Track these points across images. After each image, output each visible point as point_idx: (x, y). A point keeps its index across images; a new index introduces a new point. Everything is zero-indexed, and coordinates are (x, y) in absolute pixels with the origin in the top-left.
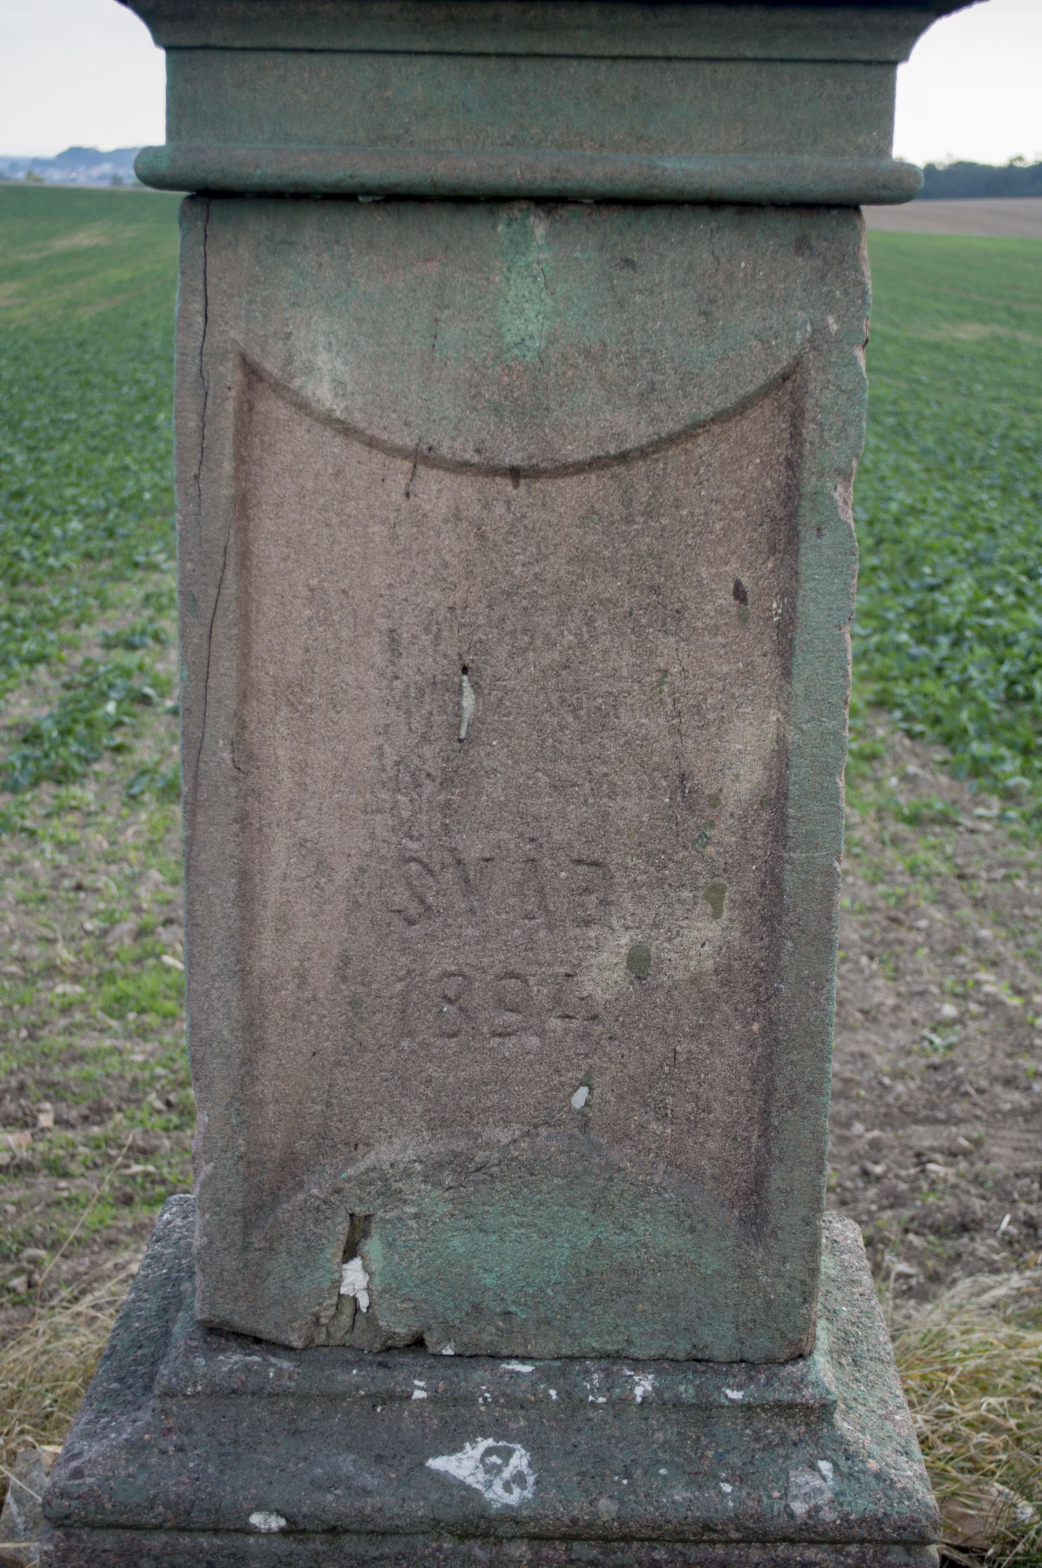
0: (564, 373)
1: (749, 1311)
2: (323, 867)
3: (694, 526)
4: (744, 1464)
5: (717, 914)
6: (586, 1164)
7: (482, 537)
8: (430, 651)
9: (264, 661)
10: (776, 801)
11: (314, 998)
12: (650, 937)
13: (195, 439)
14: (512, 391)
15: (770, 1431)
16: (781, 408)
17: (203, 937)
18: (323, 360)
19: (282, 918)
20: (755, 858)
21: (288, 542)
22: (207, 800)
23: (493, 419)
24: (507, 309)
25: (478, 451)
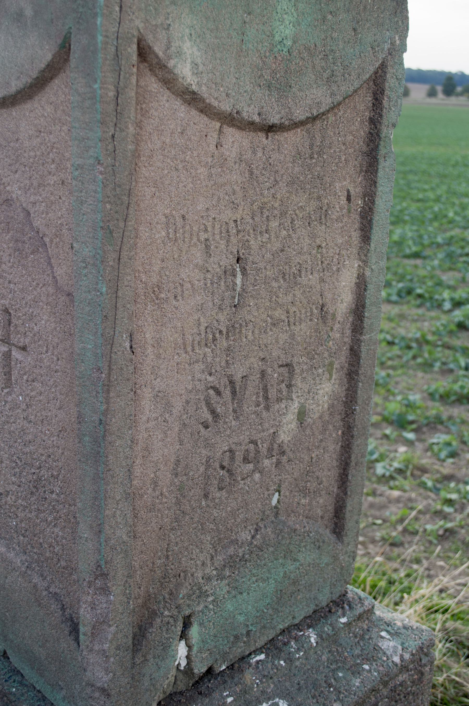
1: (335, 576)
2: (168, 406)
3: (335, 159)
4: (361, 651)
5: (330, 379)
7: (251, 173)
10: (359, 310)
11: (162, 494)
13: (112, 106)
14: (276, 74)
15: (357, 630)
17: (113, 477)
19: (146, 449)
20: (345, 343)
22: (116, 380)
24: (277, 18)
25: (259, 114)
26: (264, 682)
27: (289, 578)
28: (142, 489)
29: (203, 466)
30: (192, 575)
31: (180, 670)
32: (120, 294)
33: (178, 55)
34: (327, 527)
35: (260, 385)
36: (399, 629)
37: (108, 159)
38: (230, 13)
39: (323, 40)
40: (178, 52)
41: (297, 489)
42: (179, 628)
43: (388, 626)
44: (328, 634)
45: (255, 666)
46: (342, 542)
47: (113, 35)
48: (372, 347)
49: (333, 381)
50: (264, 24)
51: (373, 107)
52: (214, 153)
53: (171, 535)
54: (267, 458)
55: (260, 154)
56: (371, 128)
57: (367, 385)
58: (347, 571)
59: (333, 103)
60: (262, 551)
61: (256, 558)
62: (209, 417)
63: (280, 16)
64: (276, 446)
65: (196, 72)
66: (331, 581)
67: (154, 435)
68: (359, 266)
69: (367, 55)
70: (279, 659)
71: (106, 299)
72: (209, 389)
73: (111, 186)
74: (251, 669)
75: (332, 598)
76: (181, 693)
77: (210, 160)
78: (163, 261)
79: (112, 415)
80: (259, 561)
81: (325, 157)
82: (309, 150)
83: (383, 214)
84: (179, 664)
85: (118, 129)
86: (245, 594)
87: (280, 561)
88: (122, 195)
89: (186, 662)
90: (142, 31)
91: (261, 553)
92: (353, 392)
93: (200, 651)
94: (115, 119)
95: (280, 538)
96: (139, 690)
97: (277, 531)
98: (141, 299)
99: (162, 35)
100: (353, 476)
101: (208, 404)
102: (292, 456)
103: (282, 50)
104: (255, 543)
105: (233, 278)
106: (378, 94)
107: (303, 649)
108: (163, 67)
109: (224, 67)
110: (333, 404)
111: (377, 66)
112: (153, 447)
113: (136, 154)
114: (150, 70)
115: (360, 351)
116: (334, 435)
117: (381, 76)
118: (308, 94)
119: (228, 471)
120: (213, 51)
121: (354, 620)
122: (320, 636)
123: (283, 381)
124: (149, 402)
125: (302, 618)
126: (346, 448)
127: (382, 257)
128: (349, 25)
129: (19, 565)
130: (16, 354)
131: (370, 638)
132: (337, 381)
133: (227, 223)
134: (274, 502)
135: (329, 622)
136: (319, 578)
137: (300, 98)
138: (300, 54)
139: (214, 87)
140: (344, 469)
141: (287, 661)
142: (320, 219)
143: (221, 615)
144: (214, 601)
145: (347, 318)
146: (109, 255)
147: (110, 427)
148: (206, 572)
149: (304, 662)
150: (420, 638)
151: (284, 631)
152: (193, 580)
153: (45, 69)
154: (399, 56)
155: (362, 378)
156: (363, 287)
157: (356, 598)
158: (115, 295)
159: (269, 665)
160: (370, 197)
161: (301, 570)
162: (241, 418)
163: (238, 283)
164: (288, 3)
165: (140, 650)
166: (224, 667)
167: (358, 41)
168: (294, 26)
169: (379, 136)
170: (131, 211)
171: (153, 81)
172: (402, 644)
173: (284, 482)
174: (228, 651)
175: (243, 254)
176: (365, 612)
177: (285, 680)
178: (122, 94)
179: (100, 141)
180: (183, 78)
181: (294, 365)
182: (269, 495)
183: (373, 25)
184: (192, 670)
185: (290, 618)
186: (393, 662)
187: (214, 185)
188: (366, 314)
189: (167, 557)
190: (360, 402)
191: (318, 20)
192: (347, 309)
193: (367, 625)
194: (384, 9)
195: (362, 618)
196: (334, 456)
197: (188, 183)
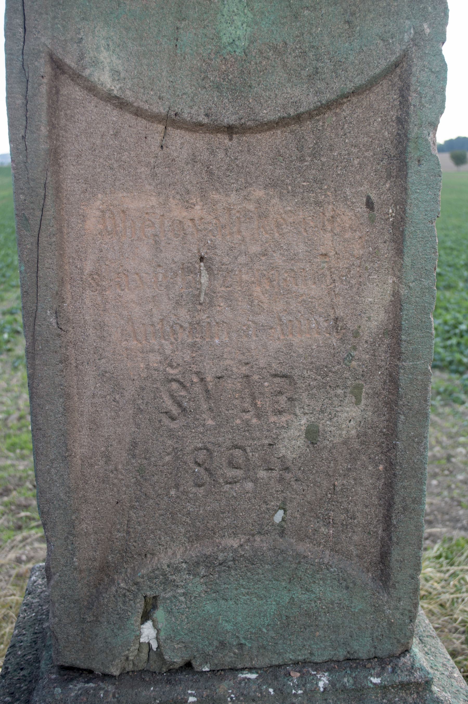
0: (261, 62)
1: (380, 630)
3: (341, 162)
5: (358, 402)
6: (284, 555)
7: (210, 173)
8: (180, 248)
9: (74, 259)
10: (394, 331)
11: (116, 470)
12: (319, 418)
14: (228, 75)
15: (397, 699)
16: (393, 85)
17: (44, 436)
18: (104, 56)
20: (380, 367)
24: (223, 20)
25: (207, 115)
30: (158, 559)
32: (40, 274)
33: (93, 64)
39: (297, 36)
49: (362, 406)
51: (400, 105)
52: (157, 154)
58: (401, 630)
62: (175, 411)
65: (117, 78)
66: (372, 634)
67: (102, 411)
68: (394, 282)
69: (372, 47)
70: (270, 686)
77: (152, 160)
90: (49, 46)
94: (25, 123)
96: (91, 647)
101: (172, 396)
102: (300, 474)
107: (304, 688)
108: (79, 76)
112: (102, 423)
114: (72, 80)
117: (406, 70)
119: (206, 469)
135: (354, 675)
137: (265, 97)
142: (323, 226)
143: (197, 612)
144: (184, 594)
146: (25, 239)
156: (399, 306)
164: (238, 4)
169: (406, 136)
171: (77, 89)
178: (31, 102)
180: (102, 85)
181: (295, 378)
187: (159, 184)
189: (128, 533)
193: (413, 699)
195: (409, 689)
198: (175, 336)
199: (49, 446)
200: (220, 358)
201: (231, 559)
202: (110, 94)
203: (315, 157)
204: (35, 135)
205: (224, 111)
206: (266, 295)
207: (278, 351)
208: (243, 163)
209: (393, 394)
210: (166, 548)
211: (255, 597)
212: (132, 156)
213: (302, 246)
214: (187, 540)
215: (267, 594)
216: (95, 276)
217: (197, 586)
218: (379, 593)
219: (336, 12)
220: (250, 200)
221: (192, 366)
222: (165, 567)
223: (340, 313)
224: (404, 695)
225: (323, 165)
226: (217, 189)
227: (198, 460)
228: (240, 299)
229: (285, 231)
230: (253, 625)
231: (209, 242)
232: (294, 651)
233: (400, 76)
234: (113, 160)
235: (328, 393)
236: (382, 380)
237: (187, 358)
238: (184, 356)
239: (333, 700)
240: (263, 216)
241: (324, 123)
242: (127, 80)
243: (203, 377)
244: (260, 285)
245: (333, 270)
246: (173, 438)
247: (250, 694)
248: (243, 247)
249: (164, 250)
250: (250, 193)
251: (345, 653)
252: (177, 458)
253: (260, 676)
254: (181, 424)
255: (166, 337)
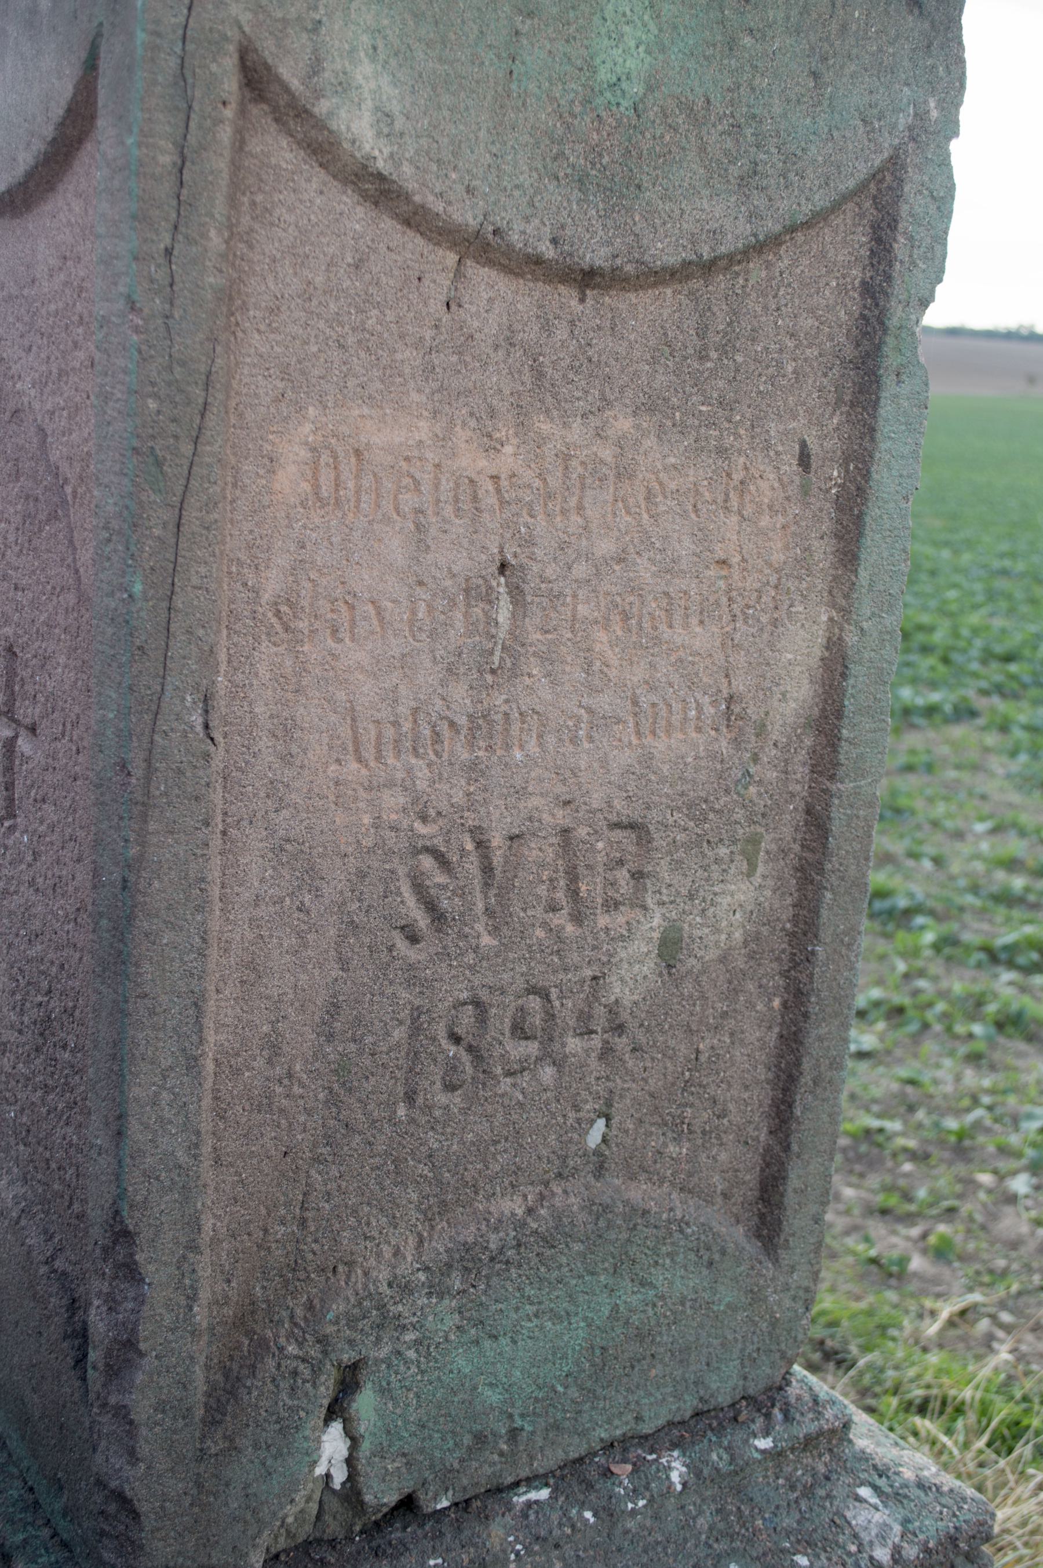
0: (662, 137)
1: (756, 1339)
2: (311, 877)
3: (768, 367)
4: (799, 1522)
5: (750, 873)
6: (610, 1216)
7: (539, 374)
8: (465, 542)
9: (240, 563)
10: (828, 721)
11: (290, 1075)
12: (684, 912)
13: (166, 188)
14: (600, 155)
15: (800, 1472)
16: (862, 216)
17: (152, 1013)
18: (365, 74)
20: (793, 795)
21: (285, 373)
22: (166, 794)
23: (576, 194)
24: (603, 31)
25: (554, 241)
26: (536, 1553)
27: (627, 1323)
28: (238, 1054)
29: (403, 1028)
30: (366, 1274)
31: (334, 1491)
32: (178, 602)
33: (339, 89)
34: (738, 1222)
35: (560, 862)
36: (905, 1486)
37: (153, 300)
38: (479, 9)
39: (729, 90)
40: (340, 84)
41: (657, 1119)
42: (322, 1389)
43: (880, 1476)
44: (717, 1470)
45: (522, 1511)
46: (776, 1261)
47: (174, 32)
48: (861, 812)
49: (757, 880)
50: (567, 41)
51: (870, 257)
52: (440, 320)
53: (313, 1172)
54: (576, 1035)
55: (561, 333)
56: (865, 306)
57: (847, 898)
58: (789, 1331)
59: (755, 235)
60: (554, 1247)
61: (535, 1260)
62: (422, 921)
63: (613, 27)
64: (600, 1011)
65: (386, 130)
66: (742, 1350)
67: (271, 936)
69: (848, 135)
70: (583, 1505)
71: (141, 609)
72: (419, 852)
73: (160, 360)
74: (508, 1518)
75: (744, 1388)
76: (332, 1543)
77: (429, 334)
78: (303, 547)
79: (153, 872)
80: (543, 1269)
81: (739, 359)
82: (695, 337)
83: (892, 505)
84: (328, 1476)
85: (180, 237)
86: (504, 1341)
87: (602, 1278)
88: (188, 384)
89: (346, 1474)
90: (247, 29)
91: (548, 1252)
92: (810, 911)
93: (380, 1453)
94: (174, 215)
95: (602, 1223)
96: (213, 1515)
97: (595, 1208)
98: (244, 624)
99: (299, 41)
100: (805, 1109)
101: (419, 888)
102: (642, 1038)
103: (618, 104)
104: (534, 1225)
105: (488, 607)
106: (882, 229)
107: (648, 1494)
108: (303, 114)
109: (462, 127)
110: (758, 933)
111: (877, 163)
112: (270, 964)
113: (230, 298)
114: (276, 120)
115: (829, 818)
116: (759, 1007)
117: (890, 188)
118: (688, 209)
119: (470, 1049)
120: (434, 89)
121: (793, 1449)
122: (694, 1470)
123: (621, 863)
124: (260, 860)
125: (661, 1422)
126: (791, 1041)
127: (891, 606)
128: (800, 65)
129: (10, 1205)
130: (24, 745)
131: (829, 1496)
132: (770, 882)
133: (471, 481)
134: (594, 1137)
136: (709, 1336)
137: (663, 215)
138: (665, 116)
139: (435, 168)
140: (785, 1090)
141: (602, 1514)
142: (726, 501)
143: (439, 1378)
144: (418, 1342)
145: (798, 736)
146: (151, 512)
147: (147, 899)
148: (398, 1272)
149: (648, 1523)
150: (955, 1515)
151: (612, 1445)
152: (365, 1287)
153: (65, 118)
154: (938, 146)
155: (833, 879)
156: (840, 669)
157: (807, 1397)
158: (165, 604)
159: (555, 1517)
160: (859, 461)
161: (659, 1310)
162: (505, 930)
163: (501, 620)
165: (220, 1422)
166: (445, 1503)
167: (826, 103)
168: (648, 52)
169: (882, 323)
170: (211, 420)
171: (284, 144)
172: (906, 1522)
173: (621, 1096)
174: (456, 1465)
175: (515, 556)
176: (820, 1433)
177: (595, 1558)
178: (193, 163)
179: (136, 259)
180: (354, 142)
181: (651, 828)
182: (579, 1121)
183: (866, 70)
184: (359, 1493)
185: (629, 1417)
186: (871, 1558)
187: (438, 391)
188: (844, 731)
189: (303, 1223)
190: (826, 935)
191: (714, 45)
192: (798, 716)
193: (826, 1464)
194: (897, 36)
195: (816, 1447)
196: (761, 1056)
197: (371, 380)
198: (437, 747)
199: (161, 1035)
200: (522, 793)
201: (514, 1243)
202: (365, 167)
203: (726, 353)
204: (194, 249)
205: (588, 236)
206: (617, 650)
207: (628, 771)
208: (600, 355)
209: (813, 851)
210: (378, 1245)
211: (550, 1319)
212: (388, 319)
213: (687, 542)
214: (421, 1217)
215: (572, 1308)
216: (284, 608)
217: (443, 1318)
218: (760, 1263)
219: (797, 50)
220: (606, 438)
221: (466, 814)
222: (384, 1288)
223: (739, 685)
224: (810, 1460)
225: (737, 370)
226: (547, 411)
227: (458, 1030)
228: (569, 659)
229: (662, 508)
230: (541, 1381)
231: (523, 530)
232: (609, 1422)
233: (875, 198)
234: (347, 327)
235: (704, 856)
236: (794, 823)
237: (459, 797)
238: (452, 792)
239: (695, 1504)
240: (624, 474)
241: (747, 280)
242: (407, 138)
243: (484, 838)
244: (606, 627)
245: (734, 594)
246: (414, 984)
247: (554, 1533)
248: (584, 543)
249: (433, 547)
250: (607, 422)
251: (695, 1402)
252: (416, 1030)
253: (555, 1490)
254: (432, 950)
255: (421, 751)
